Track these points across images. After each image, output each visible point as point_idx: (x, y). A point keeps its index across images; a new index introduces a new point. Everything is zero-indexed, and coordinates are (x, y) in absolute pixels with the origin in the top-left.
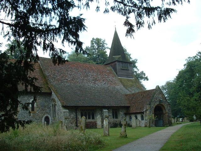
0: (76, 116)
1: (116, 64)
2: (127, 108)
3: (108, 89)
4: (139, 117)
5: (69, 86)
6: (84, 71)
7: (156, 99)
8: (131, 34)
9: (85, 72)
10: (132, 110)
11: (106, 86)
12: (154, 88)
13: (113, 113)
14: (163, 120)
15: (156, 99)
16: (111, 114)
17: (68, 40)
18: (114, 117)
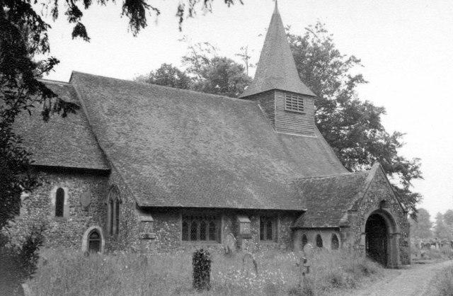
2: (297, 214)
10: (308, 221)
16: (258, 230)
17: (300, 39)
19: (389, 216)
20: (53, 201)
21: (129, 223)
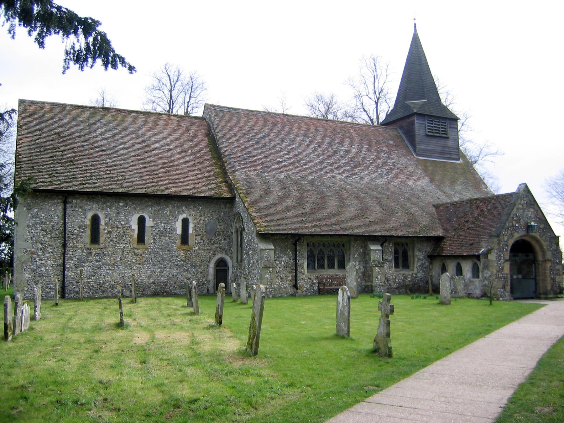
0: (295, 259)
1: (413, 123)
3: (388, 189)
4: (467, 268)
5: (282, 180)
6: (327, 140)
7: (518, 221)
8: (558, 199)
9: (329, 144)
10: (448, 248)
11: (382, 181)
12: (512, 189)
13: (396, 252)
14: (535, 279)
15: (518, 221)
16: (391, 257)
18: (400, 264)
19: (537, 241)
20: (179, 231)
21: (251, 251)
